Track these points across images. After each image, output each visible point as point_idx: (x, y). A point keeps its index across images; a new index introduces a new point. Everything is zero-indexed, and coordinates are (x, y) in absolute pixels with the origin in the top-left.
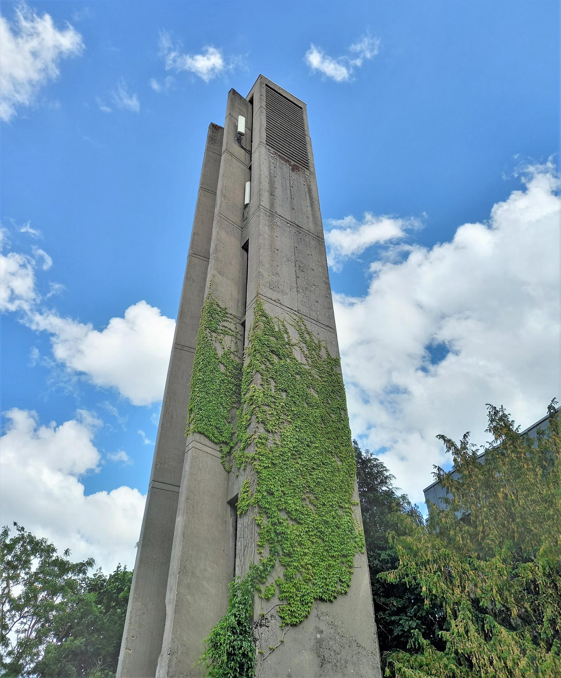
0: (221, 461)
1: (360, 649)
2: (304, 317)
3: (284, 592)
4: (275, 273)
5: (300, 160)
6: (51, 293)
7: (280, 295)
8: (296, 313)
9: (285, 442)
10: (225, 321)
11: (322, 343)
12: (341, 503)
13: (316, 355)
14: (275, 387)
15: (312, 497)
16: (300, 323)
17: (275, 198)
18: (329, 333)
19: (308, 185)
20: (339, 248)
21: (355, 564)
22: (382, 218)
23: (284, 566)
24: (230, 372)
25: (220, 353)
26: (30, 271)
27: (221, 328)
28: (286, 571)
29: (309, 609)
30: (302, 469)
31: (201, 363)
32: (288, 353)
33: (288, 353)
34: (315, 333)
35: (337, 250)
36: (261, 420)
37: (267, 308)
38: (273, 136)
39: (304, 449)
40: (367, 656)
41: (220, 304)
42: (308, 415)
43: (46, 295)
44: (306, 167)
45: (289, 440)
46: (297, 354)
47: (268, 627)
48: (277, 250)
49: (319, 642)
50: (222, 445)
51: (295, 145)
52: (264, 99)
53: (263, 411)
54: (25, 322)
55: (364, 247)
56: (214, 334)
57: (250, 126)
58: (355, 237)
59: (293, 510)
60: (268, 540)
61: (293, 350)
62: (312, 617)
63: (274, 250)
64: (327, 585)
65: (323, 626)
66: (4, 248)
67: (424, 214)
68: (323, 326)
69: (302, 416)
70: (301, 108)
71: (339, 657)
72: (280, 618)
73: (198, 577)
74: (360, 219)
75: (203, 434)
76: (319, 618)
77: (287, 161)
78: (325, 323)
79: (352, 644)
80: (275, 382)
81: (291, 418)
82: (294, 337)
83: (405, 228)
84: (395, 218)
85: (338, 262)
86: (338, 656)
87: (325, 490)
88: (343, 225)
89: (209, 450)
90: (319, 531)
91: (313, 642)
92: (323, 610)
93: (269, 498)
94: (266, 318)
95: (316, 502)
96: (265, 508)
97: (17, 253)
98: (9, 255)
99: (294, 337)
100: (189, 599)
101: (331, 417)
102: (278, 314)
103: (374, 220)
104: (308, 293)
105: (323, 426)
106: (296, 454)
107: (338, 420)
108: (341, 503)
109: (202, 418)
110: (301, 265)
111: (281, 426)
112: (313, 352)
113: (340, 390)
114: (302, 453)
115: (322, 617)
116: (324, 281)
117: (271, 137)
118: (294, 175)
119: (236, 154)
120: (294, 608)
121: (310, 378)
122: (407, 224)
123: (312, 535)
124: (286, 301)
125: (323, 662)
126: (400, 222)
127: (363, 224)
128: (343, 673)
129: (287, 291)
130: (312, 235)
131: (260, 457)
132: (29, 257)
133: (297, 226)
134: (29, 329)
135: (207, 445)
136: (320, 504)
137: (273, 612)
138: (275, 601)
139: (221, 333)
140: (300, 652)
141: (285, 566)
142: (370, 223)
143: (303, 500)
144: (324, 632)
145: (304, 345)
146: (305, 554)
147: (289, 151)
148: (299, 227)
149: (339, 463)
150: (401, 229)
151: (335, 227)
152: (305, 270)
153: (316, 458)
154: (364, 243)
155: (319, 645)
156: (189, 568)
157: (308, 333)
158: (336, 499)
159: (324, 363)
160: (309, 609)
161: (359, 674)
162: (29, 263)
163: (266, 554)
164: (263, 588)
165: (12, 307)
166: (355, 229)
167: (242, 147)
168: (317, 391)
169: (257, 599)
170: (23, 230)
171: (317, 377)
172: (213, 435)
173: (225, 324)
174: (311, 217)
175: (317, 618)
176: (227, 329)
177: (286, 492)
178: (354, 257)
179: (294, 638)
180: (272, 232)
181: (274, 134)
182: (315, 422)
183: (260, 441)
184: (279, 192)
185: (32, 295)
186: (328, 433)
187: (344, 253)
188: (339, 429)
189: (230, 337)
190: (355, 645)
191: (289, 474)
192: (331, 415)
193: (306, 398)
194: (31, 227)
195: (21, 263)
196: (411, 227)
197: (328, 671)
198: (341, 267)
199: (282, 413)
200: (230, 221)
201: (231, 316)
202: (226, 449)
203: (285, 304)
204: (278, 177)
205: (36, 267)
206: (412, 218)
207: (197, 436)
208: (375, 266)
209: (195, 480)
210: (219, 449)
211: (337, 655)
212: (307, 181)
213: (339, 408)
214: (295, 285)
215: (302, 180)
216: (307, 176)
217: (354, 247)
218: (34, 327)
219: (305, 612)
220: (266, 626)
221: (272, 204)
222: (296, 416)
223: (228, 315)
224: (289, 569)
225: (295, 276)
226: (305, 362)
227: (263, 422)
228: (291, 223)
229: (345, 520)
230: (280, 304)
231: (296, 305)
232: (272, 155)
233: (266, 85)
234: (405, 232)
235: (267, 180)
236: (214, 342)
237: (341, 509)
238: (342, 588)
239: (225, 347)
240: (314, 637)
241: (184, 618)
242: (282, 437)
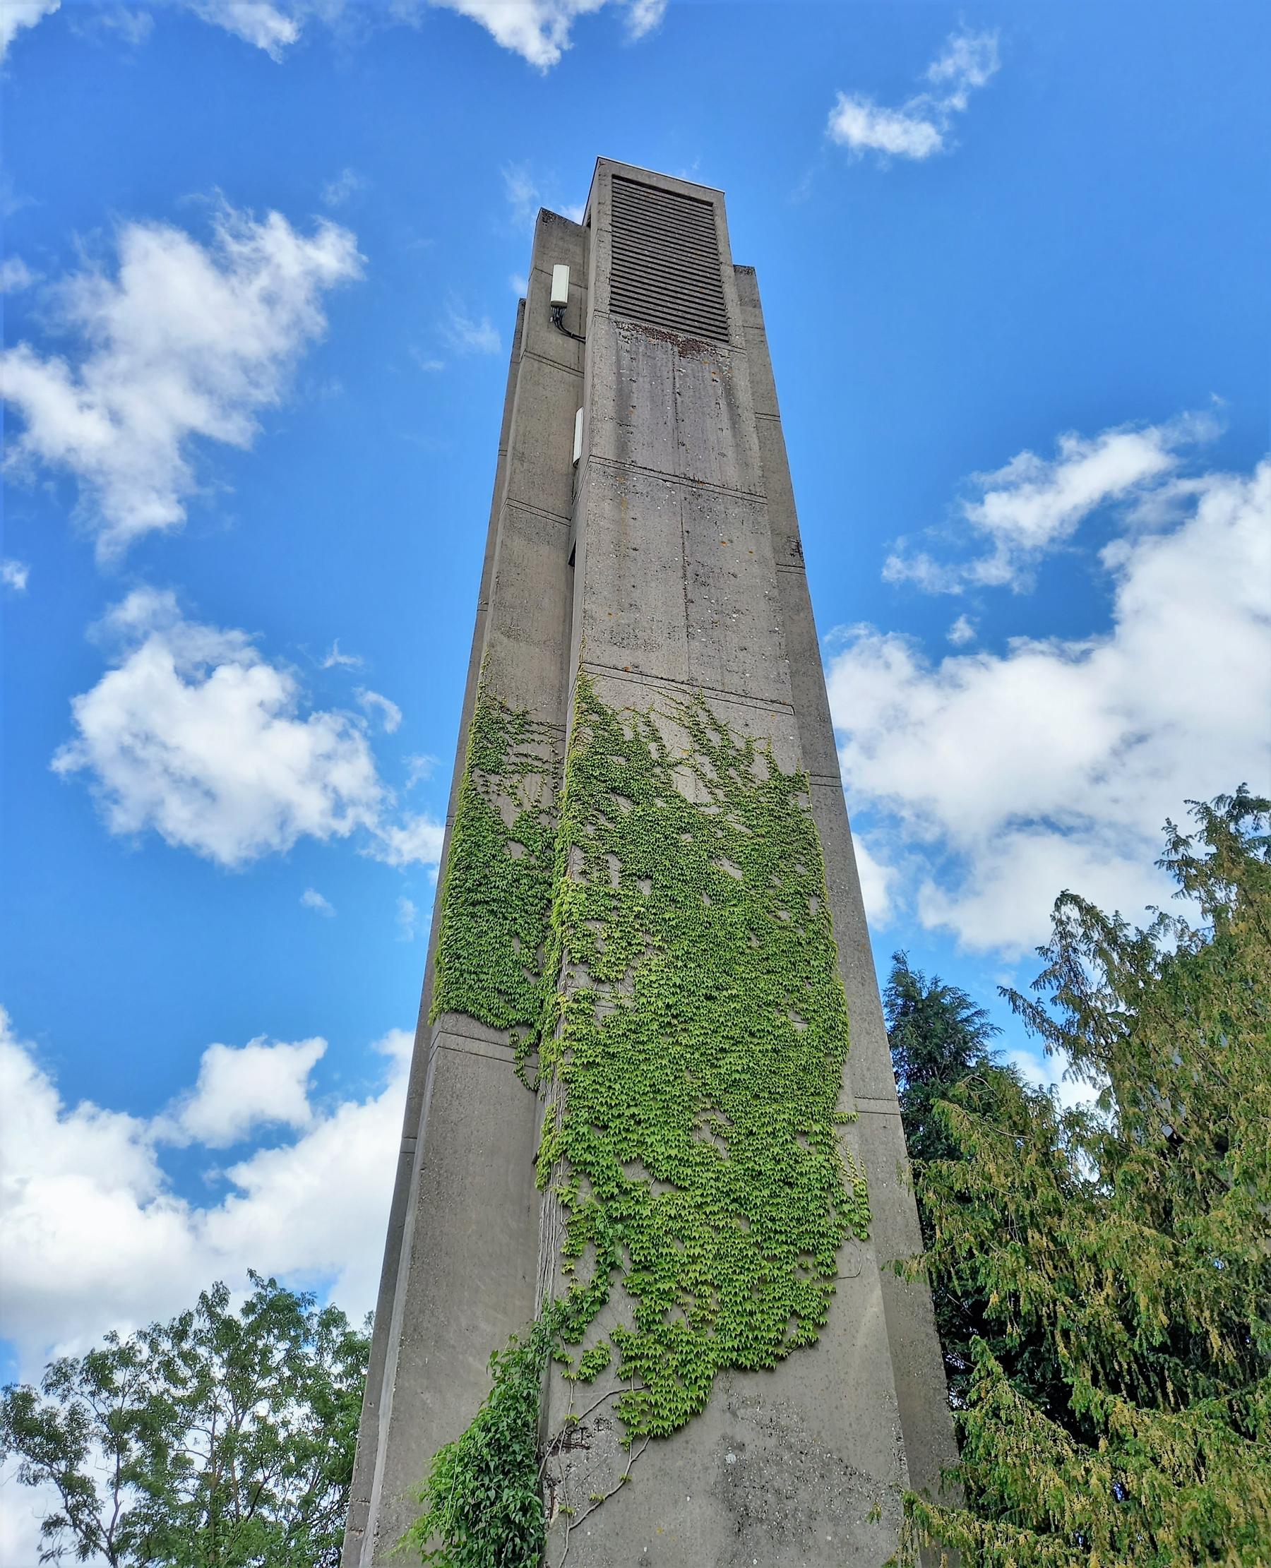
0: (515, 1067)
1: (852, 1482)
2: (706, 692)
3: (631, 1358)
4: (627, 606)
5: (704, 326)
6: (414, 778)
7: (639, 653)
8: (683, 687)
9: (643, 1000)
10: (523, 741)
11: (755, 745)
12: (800, 1123)
13: (739, 775)
14: (621, 872)
15: (720, 1119)
16: (696, 709)
17: (631, 429)
18: (777, 718)
19: (723, 379)
20: (1015, 535)
21: (842, 1268)
22: (1103, 438)
23: (634, 1295)
24: (538, 858)
25: (510, 817)
26: (362, 745)
27: (514, 759)
28: (639, 1307)
29: (702, 1392)
30: (688, 1056)
31: (459, 850)
32: (659, 785)
33: (659, 785)
34: (737, 726)
35: (1012, 540)
36: (579, 955)
37: (603, 692)
38: (630, 288)
39: (697, 1008)
40: (873, 1497)
41: (511, 704)
42: (710, 924)
43: (405, 786)
44: (721, 337)
45: (656, 991)
46: (686, 786)
47: (588, 1448)
48: (635, 549)
49: (733, 1476)
50: (517, 1030)
51: (692, 293)
52: (609, 211)
53: (584, 935)
54: (373, 852)
55: (1076, 517)
56: (494, 779)
57: (579, 280)
58: (1048, 498)
59: (660, 1158)
60: (591, 1239)
61: (674, 775)
62: (714, 1414)
63: (624, 551)
64: (753, 1329)
65: (743, 1433)
66: (300, 706)
67: (1215, 398)
68: (760, 704)
69: (693, 930)
70: (711, 204)
71: (790, 1505)
72: (620, 1424)
73: (454, 1347)
74: (1051, 454)
75: (465, 1012)
76: (734, 1414)
77: (665, 337)
78: (767, 695)
79: (830, 1471)
80: (620, 860)
81: (662, 939)
82: (677, 742)
83: (1170, 445)
84: (1138, 429)
85: (1021, 570)
86: (790, 1502)
87: (757, 1097)
88: (1012, 478)
89: (482, 1048)
90: (734, 1200)
91: (714, 1475)
92: (747, 1393)
93: (596, 1138)
94: (601, 713)
95: (731, 1131)
96: (585, 1163)
97: (325, 711)
98: (311, 719)
99: (677, 742)
100: (428, 1401)
101: (779, 918)
102: (632, 699)
103: (1084, 448)
104: (716, 633)
105: (755, 943)
106: (673, 1020)
107: (797, 922)
108: (800, 1123)
109: (462, 975)
110: (701, 572)
111: (637, 963)
112: (732, 772)
113: (805, 849)
114: (691, 1019)
115: (742, 1411)
116: (766, 596)
117: (625, 293)
118: (687, 366)
119: (552, 354)
120: (657, 1397)
121: (720, 834)
122: (1175, 436)
123: (714, 1213)
124: (656, 664)
125: (742, 1521)
126: (1155, 434)
127: (1061, 464)
128: (801, 1544)
129: (660, 640)
130: (732, 493)
131: (575, 1043)
132: (350, 714)
133: (690, 483)
134: (383, 865)
135: (476, 1036)
136: (739, 1134)
137: (604, 1411)
138: (608, 1383)
139: (513, 772)
140: (676, 1502)
141: (637, 1294)
142: (1076, 458)
143: (691, 1129)
144: (750, 1448)
145: (706, 760)
146: (694, 1259)
147: (675, 312)
148: (698, 482)
149: (800, 1027)
150: (1161, 449)
151: (995, 488)
152: (710, 581)
153: (729, 1024)
154: (1075, 508)
155: (733, 1481)
156: (427, 1329)
157: (718, 729)
158: (786, 1116)
159: (761, 792)
160: (702, 1392)
161: (849, 1544)
162: (354, 725)
163: (587, 1271)
164: (573, 1355)
165: (344, 828)
166: (1044, 480)
167: (569, 334)
168: (740, 863)
169: (558, 1385)
170: (329, 663)
171: (739, 827)
172: (490, 1010)
173: (523, 749)
174: (730, 453)
175: (728, 1414)
176: (529, 761)
177: (642, 1118)
178: (1055, 549)
179: (661, 1469)
180: (620, 510)
181: (634, 283)
182: (731, 937)
183: (575, 1006)
184: (642, 415)
185: (375, 792)
186: (767, 958)
187: (1028, 543)
188: (800, 944)
189: (537, 778)
190: (837, 1470)
191: (655, 1071)
192: (780, 913)
193: (706, 882)
194: (342, 652)
195: (339, 728)
196: (1189, 439)
197: (758, 1543)
198: (1030, 579)
199: (638, 930)
200: (534, 511)
201: (542, 729)
202: (526, 1037)
203: (654, 673)
204: (641, 379)
205: (370, 732)
206: (1186, 415)
207: (450, 1021)
208: (1111, 554)
209: (444, 1122)
210: (508, 1041)
211: (785, 1501)
212: (721, 371)
213: (798, 892)
214: (682, 622)
215: (708, 372)
216: (721, 359)
217: (1050, 523)
218: (392, 860)
219: (689, 1403)
220: (583, 1447)
221: (622, 447)
222: (674, 933)
223: (534, 727)
224: (646, 1301)
225: (682, 601)
226: (708, 799)
227: (584, 961)
228: (675, 479)
229: (810, 1164)
230: (641, 673)
231: (685, 668)
232: (628, 333)
233: (614, 177)
234: (1173, 455)
235: (612, 394)
236: (493, 797)
237: (804, 1139)
238: (801, 1332)
239: (525, 801)
240: (717, 1462)
241: (414, 1446)
242: (638, 987)
